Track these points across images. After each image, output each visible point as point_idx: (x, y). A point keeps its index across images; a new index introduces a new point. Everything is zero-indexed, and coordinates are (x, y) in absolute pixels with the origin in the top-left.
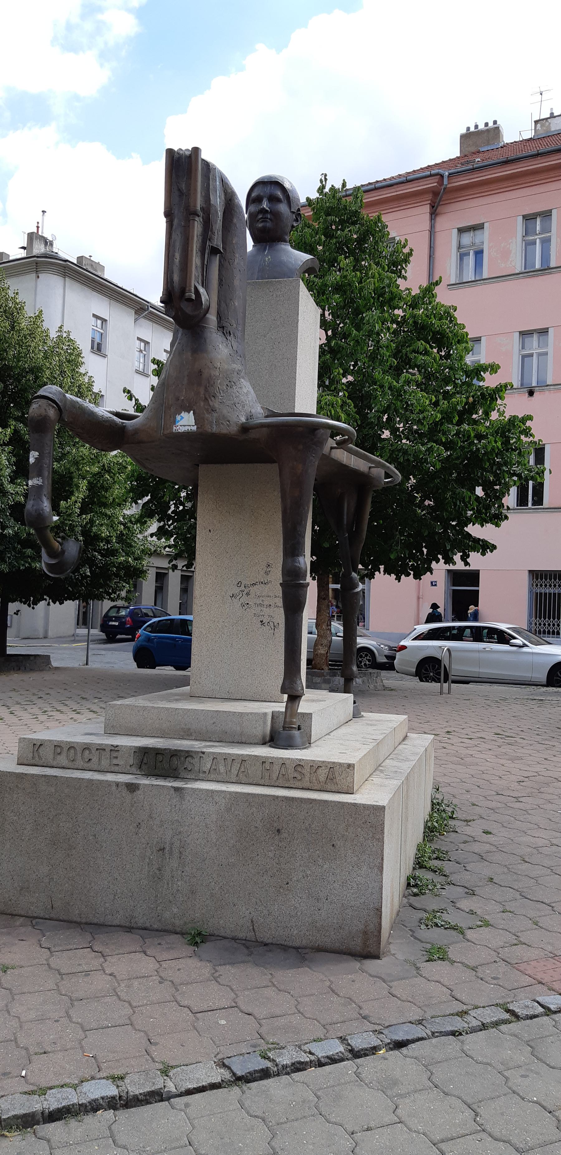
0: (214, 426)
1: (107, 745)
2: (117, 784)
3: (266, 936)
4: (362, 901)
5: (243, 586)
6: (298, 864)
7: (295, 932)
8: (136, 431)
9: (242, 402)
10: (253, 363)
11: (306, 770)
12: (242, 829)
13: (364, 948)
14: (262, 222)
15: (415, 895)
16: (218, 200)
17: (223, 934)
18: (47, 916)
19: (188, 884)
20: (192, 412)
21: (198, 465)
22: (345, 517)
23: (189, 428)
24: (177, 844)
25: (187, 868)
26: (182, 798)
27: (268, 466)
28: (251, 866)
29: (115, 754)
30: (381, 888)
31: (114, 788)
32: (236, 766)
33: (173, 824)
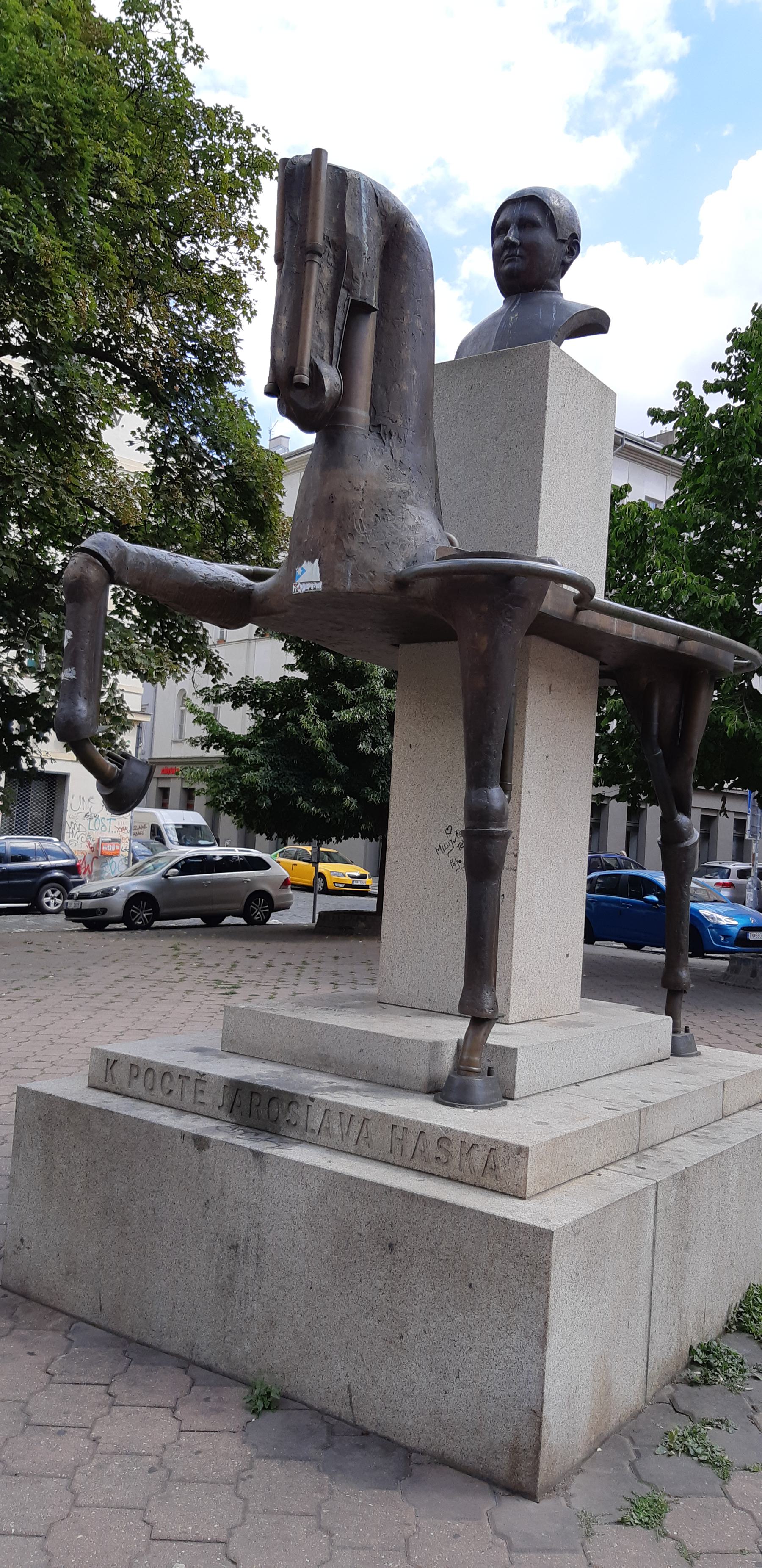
0: (349, 582)
1: (191, 1071)
2: (183, 1135)
3: (367, 1419)
4: (512, 1391)
5: (454, 833)
6: (417, 1308)
7: (410, 1423)
8: (267, 595)
9: (401, 540)
10: (478, 483)
11: (455, 1148)
12: (340, 1234)
13: (511, 1475)
14: (508, 262)
15: (693, 1383)
16: (365, 226)
17: (308, 1401)
18: (94, 1321)
19: (266, 1309)
20: (317, 561)
21: (398, 646)
22: (656, 723)
23: (312, 586)
24: (253, 1243)
25: (265, 1284)
26: (262, 1170)
27: (446, 644)
28: (350, 1297)
29: (200, 1087)
30: (542, 1375)
31: (179, 1140)
32: (356, 1127)
33: (250, 1209)
